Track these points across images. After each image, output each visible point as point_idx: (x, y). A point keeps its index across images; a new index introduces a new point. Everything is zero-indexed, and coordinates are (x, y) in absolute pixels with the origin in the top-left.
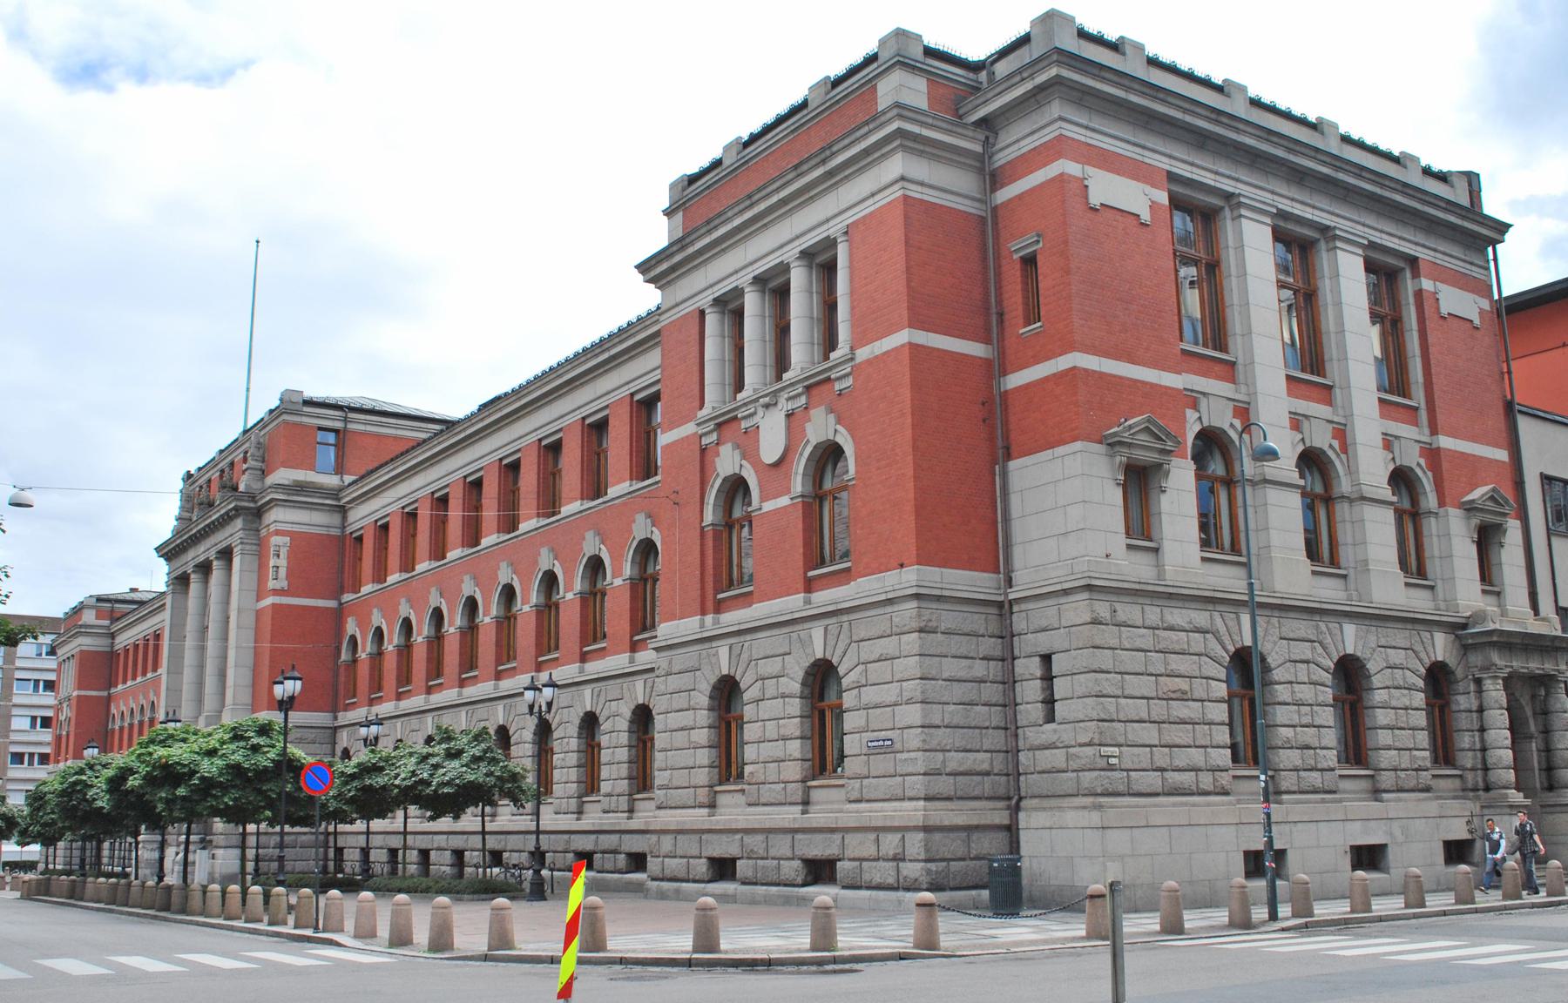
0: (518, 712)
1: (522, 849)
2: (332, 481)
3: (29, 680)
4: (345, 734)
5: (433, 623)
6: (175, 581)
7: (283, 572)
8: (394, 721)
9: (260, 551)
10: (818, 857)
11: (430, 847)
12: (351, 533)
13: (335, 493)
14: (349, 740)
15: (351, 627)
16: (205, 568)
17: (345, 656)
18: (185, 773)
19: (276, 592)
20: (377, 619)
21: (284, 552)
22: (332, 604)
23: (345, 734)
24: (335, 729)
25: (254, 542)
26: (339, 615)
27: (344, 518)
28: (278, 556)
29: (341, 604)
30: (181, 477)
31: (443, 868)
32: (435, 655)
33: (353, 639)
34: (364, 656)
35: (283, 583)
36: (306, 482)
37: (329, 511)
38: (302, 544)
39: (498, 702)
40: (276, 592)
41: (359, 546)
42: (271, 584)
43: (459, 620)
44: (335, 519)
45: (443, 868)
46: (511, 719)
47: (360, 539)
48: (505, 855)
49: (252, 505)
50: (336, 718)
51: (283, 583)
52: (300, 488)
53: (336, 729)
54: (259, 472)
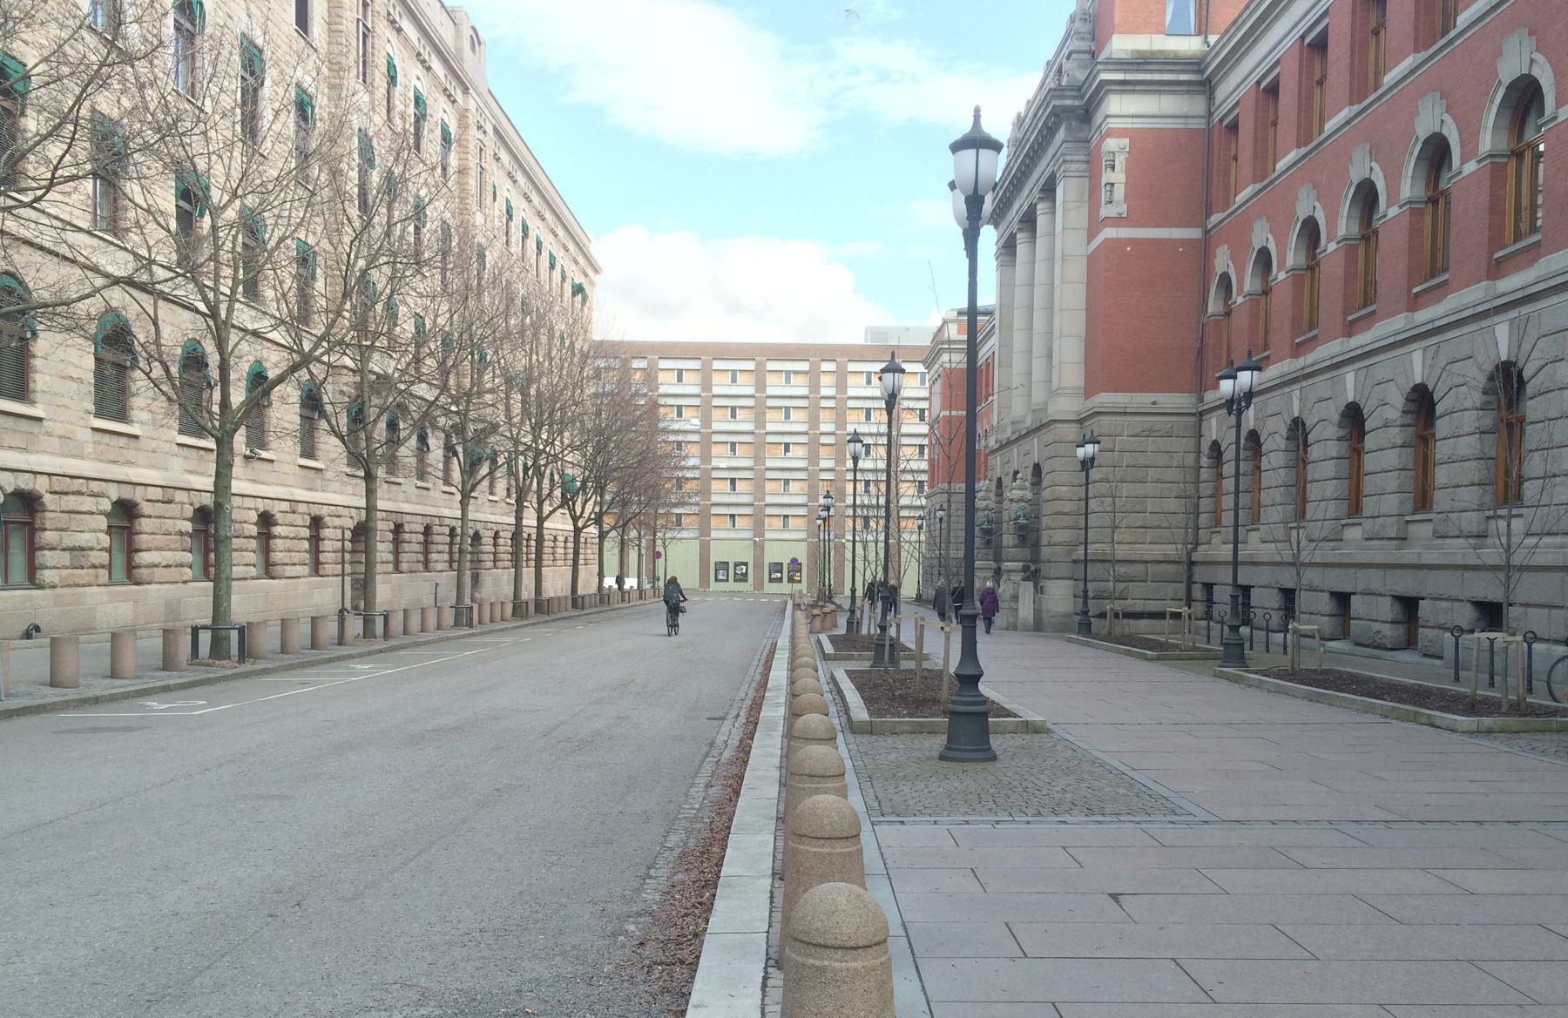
0: (1544, 330)
1: (1558, 602)
2: (1190, 45)
3: (782, 371)
4: (1214, 421)
5: (1357, 213)
6: (1002, 251)
7: (1119, 192)
8: (1287, 390)
9: (1093, 165)
10: (31, 385)
11: (1349, 589)
12: (1221, 120)
13: (1195, 64)
14: (1219, 429)
15: (1222, 261)
16: (1029, 221)
17: (1214, 306)
18: (465, 450)
19: (1118, 221)
20: (1261, 236)
21: (1120, 162)
22: (1195, 233)
23: (1214, 421)
24: (1201, 415)
25: (1083, 158)
26: (1205, 247)
27: (1211, 98)
28: (1113, 168)
29: (1207, 232)
30: (1011, 122)
31: (1376, 626)
32: (1361, 267)
33: (1225, 278)
34: (1240, 300)
35: (1122, 209)
36: (1153, 53)
37: (1187, 92)
38: (1145, 144)
39: (1496, 319)
40: (1118, 221)
41: (1233, 138)
42: (1106, 211)
43: (1410, 187)
44: (1196, 105)
45: (1376, 626)
46: (1526, 346)
47: (1234, 127)
48: (1514, 612)
49: (1077, 103)
50: (1201, 400)
51: (1122, 209)
52: (1142, 61)
53: (1201, 414)
54: (1087, 56)
